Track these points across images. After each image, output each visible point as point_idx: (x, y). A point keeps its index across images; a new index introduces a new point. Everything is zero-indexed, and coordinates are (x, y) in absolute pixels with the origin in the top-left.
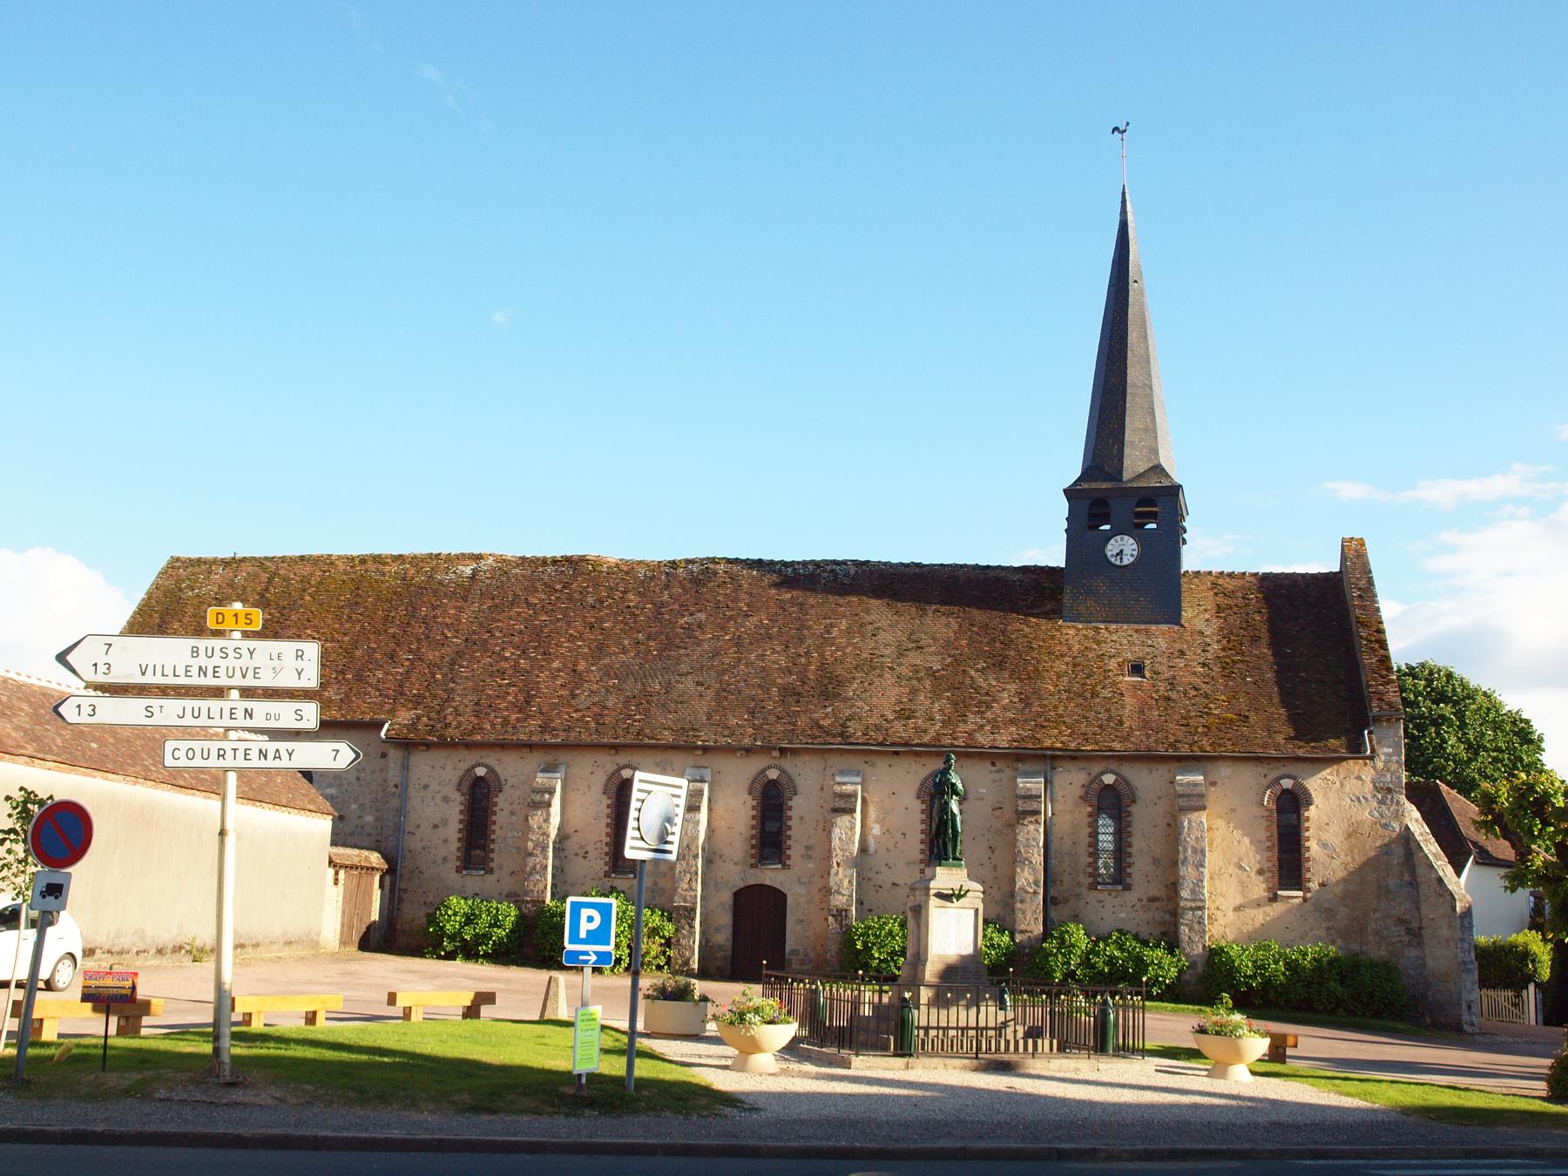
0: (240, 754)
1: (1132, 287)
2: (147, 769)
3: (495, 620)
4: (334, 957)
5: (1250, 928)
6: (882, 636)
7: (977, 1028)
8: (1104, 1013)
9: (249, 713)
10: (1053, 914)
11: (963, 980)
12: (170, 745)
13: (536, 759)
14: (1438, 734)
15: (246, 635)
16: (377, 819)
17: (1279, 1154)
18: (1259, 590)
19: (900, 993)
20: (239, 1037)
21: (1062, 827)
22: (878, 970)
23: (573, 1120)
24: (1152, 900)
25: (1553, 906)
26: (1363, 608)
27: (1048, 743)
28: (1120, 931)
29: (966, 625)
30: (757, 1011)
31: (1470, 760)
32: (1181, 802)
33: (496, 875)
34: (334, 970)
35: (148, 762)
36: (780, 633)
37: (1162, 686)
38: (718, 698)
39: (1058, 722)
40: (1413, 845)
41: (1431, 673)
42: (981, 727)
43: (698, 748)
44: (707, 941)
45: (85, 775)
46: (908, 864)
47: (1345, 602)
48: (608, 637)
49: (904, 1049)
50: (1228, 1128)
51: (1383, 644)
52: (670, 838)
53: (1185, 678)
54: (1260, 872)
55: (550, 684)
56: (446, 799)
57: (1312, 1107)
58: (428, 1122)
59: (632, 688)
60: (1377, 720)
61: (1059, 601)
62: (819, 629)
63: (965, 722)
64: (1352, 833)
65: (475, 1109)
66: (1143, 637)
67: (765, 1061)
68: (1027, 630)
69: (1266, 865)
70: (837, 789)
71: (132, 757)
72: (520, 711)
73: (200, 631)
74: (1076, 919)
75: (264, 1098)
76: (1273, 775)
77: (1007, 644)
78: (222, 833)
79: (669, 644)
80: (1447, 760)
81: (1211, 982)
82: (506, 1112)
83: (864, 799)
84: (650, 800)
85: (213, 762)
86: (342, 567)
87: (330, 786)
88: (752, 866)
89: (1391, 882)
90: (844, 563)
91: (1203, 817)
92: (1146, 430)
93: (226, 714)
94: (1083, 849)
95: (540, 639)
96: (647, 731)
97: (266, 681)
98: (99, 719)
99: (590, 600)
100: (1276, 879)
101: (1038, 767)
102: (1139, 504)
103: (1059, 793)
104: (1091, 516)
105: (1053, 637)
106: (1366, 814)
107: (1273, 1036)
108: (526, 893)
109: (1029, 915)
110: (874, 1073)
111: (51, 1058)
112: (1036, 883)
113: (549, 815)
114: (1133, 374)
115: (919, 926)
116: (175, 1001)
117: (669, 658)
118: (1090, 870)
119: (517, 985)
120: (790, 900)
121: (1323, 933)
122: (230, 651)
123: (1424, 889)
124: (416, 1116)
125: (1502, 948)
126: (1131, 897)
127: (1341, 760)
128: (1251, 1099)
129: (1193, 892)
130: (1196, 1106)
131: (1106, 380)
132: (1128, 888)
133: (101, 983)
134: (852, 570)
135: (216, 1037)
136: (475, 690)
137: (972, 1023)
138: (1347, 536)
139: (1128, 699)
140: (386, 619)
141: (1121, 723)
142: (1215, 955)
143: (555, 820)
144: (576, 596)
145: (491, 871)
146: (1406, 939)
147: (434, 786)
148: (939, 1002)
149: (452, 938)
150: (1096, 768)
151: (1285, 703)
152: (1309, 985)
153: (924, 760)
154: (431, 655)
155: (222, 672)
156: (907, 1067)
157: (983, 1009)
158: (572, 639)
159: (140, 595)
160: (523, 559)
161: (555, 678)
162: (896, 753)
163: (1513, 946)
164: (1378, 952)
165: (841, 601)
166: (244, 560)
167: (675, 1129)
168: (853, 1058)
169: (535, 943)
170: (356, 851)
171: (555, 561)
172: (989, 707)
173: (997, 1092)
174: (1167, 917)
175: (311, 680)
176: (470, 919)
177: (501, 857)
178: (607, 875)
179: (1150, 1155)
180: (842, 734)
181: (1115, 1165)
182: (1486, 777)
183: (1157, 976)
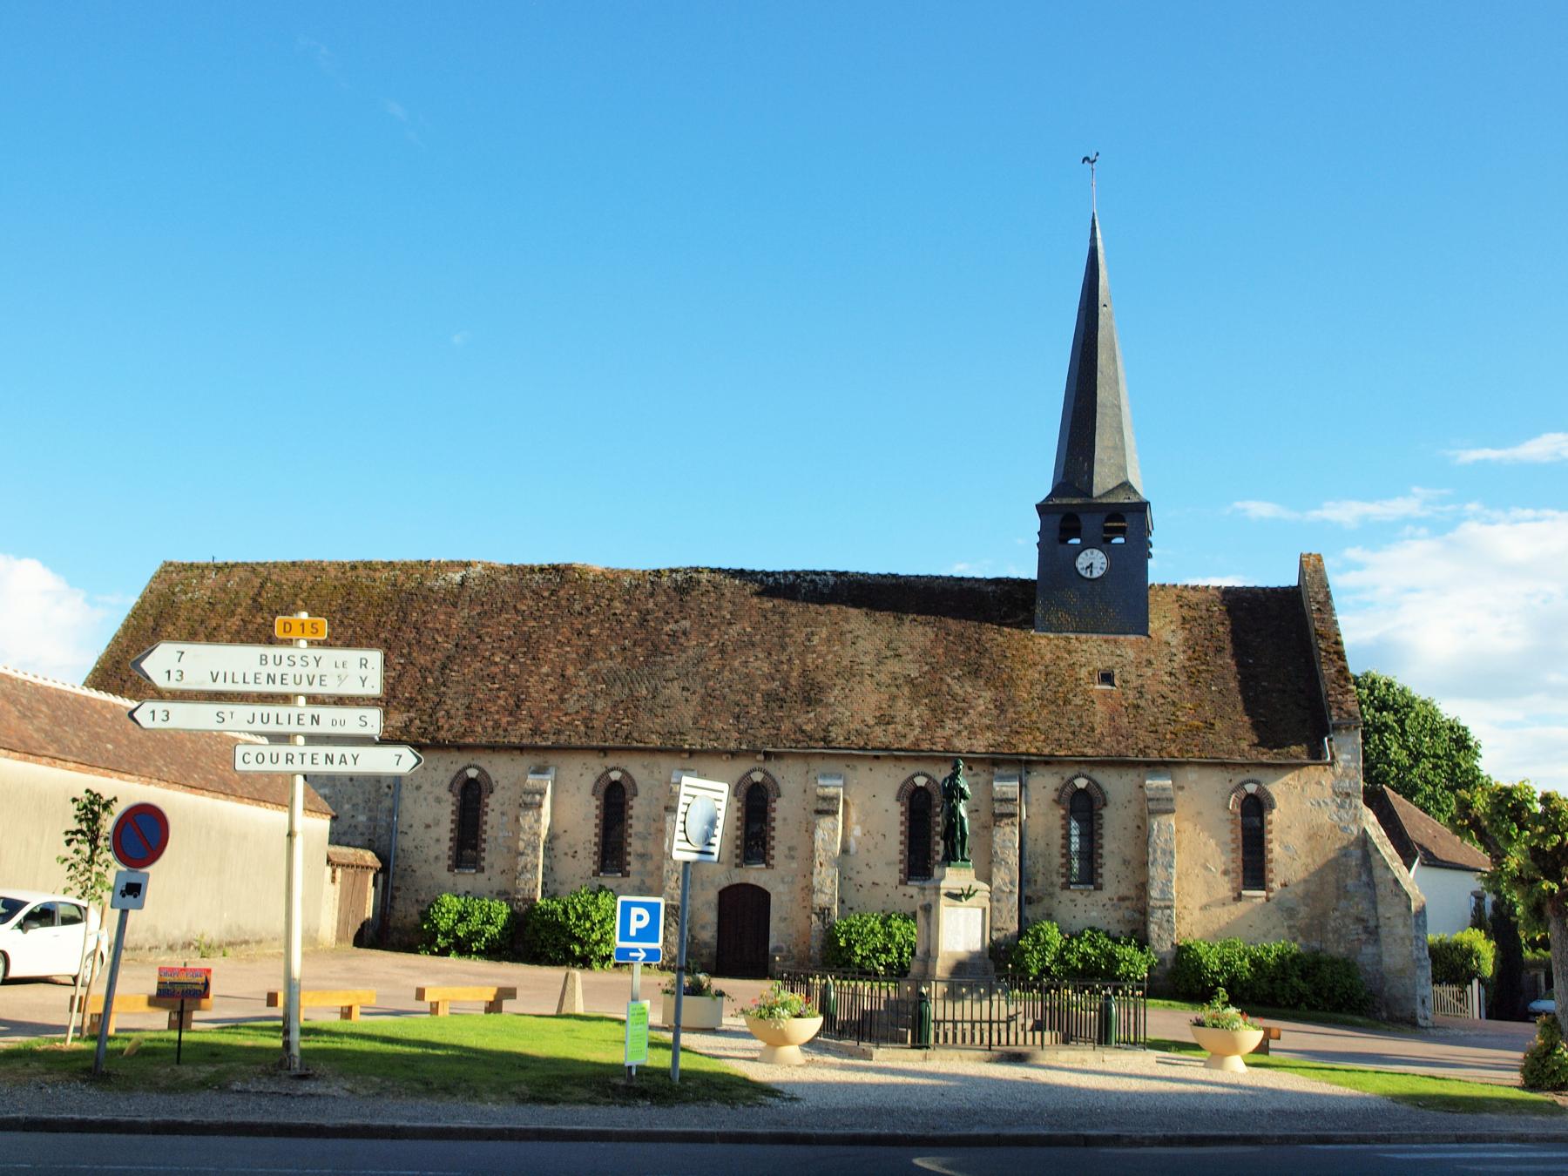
0: (308, 759)
2: (159, 770)
3: (483, 626)
4: (333, 953)
5: (1216, 927)
7: (954, 1022)
8: (1109, 1009)
9: (315, 720)
10: (1028, 913)
11: (973, 975)
12: (240, 750)
13: (527, 761)
14: (1381, 740)
15: (311, 643)
16: (370, 819)
17: (1285, 1140)
18: (1222, 602)
19: (918, 987)
21: (1036, 829)
22: (860, 966)
23: (628, 1110)
24: (1122, 899)
25: (1527, 907)
26: (1323, 621)
27: (1023, 748)
28: (1092, 929)
29: (942, 634)
30: (784, 1005)
31: (1412, 767)
32: (1151, 805)
33: (487, 873)
36: (763, 641)
37: (1131, 694)
38: (704, 704)
39: (1031, 729)
41: (1374, 682)
42: (959, 732)
44: (693, 938)
45: (103, 775)
46: (888, 864)
47: (1303, 615)
48: (595, 643)
49: (920, 1042)
50: (1235, 1116)
51: (1341, 655)
52: (713, 840)
53: (1153, 688)
54: (1225, 873)
55: (539, 688)
56: (438, 800)
57: (1309, 1095)
58: (495, 1112)
59: (618, 692)
60: (1336, 728)
61: (1032, 613)
62: (800, 638)
63: (942, 727)
64: (1313, 836)
65: (536, 1100)
66: (1112, 647)
67: (792, 1052)
68: (1000, 639)
69: (1231, 866)
70: (820, 791)
71: (145, 758)
72: (511, 714)
73: (271, 641)
74: (1049, 917)
75: (335, 1090)
78: (291, 835)
80: (1390, 765)
81: (1184, 980)
84: (696, 804)
85: (282, 766)
87: (324, 786)
88: (737, 866)
89: (1350, 882)
91: (1171, 820)
92: (1115, 448)
93: (294, 719)
94: (1056, 851)
95: (529, 645)
96: (635, 735)
97: (332, 688)
98: (173, 723)
99: (577, 607)
100: (1240, 879)
103: (1033, 799)
105: (1026, 647)
106: (1327, 816)
107: (1267, 1031)
108: (517, 892)
109: (1005, 913)
110: (892, 1066)
111: (121, 1051)
112: (1012, 883)
113: (540, 815)
114: (1102, 395)
115: (929, 924)
116: (235, 1000)
119: (535, 983)
120: (773, 899)
121: (1285, 931)
122: (297, 660)
124: (481, 1107)
125: (1448, 946)
129: (1162, 891)
130: (1202, 1095)
132: (1099, 888)
134: (832, 580)
136: (466, 694)
137: (986, 1017)
138: (1306, 552)
139: (1098, 707)
140: (378, 623)
141: (1093, 729)
144: (564, 603)
145: (482, 870)
146: (1364, 937)
147: (426, 787)
148: (953, 995)
149: (446, 935)
150: (1069, 773)
152: (1272, 980)
154: (423, 660)
155: (289, 680)
156: (925, 1058)
158: (560, 644)
159: (132, 600)
160: (511, 566)
162: (877, 757)
164: (1339, 950)
165: (821, 609)
166: (235, 565)
167: (724, 1118)
168: (875, 1050)
169: (538, 938)
170: (352, 850)
171: (542, 570)
172: (966, 713)
173: (1015, 1082)
174: (1136, 915)
175: (374, 687)
176: (462, 917)
177: (492, 856)
178: (595, 874)
179: (1168, 1141)
180: (824, 739)
181: (1134, 1151)
182: (1427, 782)
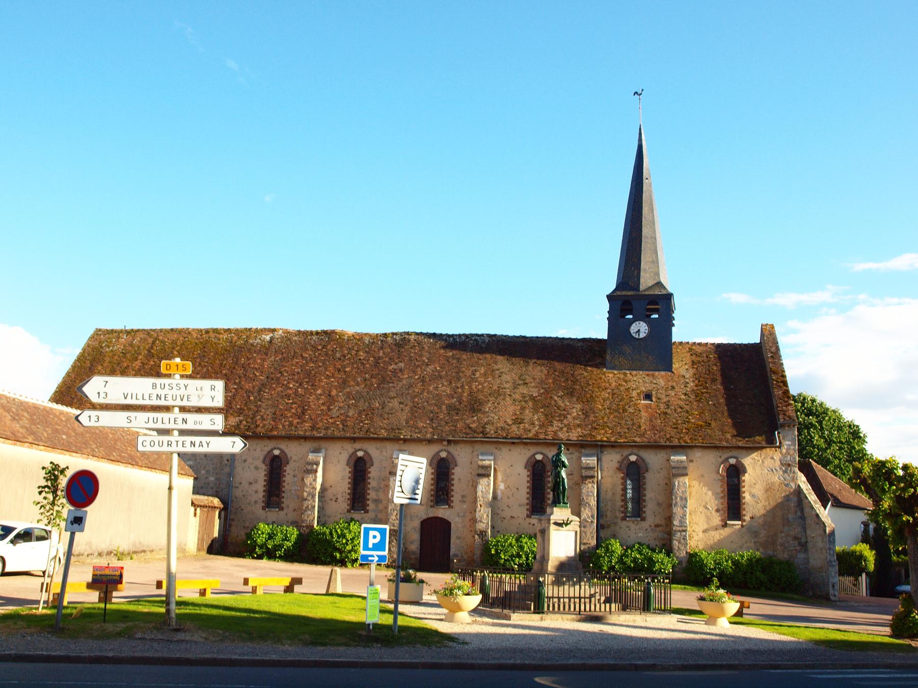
0: (180, 444)
1: (645, 182)
2: (93, 450)
3: (283, 366)
4: (195, 558)
5: (712, 542)
6: (504, 377)
9: (185, 421)
10: (602, 534)
11: (569, 571)
12: (141, 439)
13: (308, 445)
14: (809, 433)
15: (182, 376)
16: (216, 479)
18: (715, 353)
20: (180, 604)
21: (607, 484)
22: (504, 565)
23: (368, 649)
24: (657, 526)
26: (774, 363)
27: (599, 438)
29: (551, 371)
30: (459, 588)
31: (826, 449)
32: (674, 471)
33: (285, 511)
34: (198, 565)
35: (94, 446)
36: (447, 375)
37: (662, 406)
40: (802, 496)
41: (804, 399)
42: (562, 429)
43: (401, 439)
46: (520, 505)
47: (763, 360)
48: (348, 376)
49: (539, 610)
50: (723, 653)
51: (785, 383)
52: (417, 492)
53: (675, 402)
54: (717, 511)
55: (316, 402)
56: (257, 468)
57: (761, 640)
58: (290, 651)
59: (362, 405)
60: (783, 426)
61: (604, 359)
62: (469, 373)
63: (552, 426)
64: (768, 489)
65: (314, 643)
66: (651, 379)
67: (463, 616)
68: (586, 374)
69: (721, 507)
70: (480, 463)
71: (85, 444)
72: (299, 418)
73: (159, 375)
74: (614, 536)
75: (196, 638)
76: (724, 457)
77: (575, 382)
78: (170, 488)
79: (383, 380)
80: (814, 448)
81: (693, 573)
82: (331, 645)
83: (495, 469)
84: (407, 470)
85: (165, 448)
86: (195, 336)
87: (190, 460)
88: (432, 506)
89: (790, 516)
90: (482, 335)
91: (686, 480)
92: (653, 262)
93: (172, 421)
94: (618, 497)
95: (310, 377)
97: (194, 402)
98: (101, 423)
99: (338, 355)
101: (593, 451)
102: (649, 304)
104: (622, 310)
105: (600, 378)
106: (776, 478)
108: (303, 521)
110: (523, 623)
111: (71, 615)
112: (592, 516)
113: (316, 477)
114: (645, 231)
115: (544, 541)
116: (138, 582)
117: (383, 388)
118: (622, 509)
119: (314, 575)
120: (453, 526)
121: (752, 545)
122: (174, 386)
123: (808, 521)
124: (282, 648)
125: (848, 553)
126: (646, 525)
127: (762, 448)
128: (732, 636)
129: (680, 521)
130: (704, 640)
131: (631, 234)
132: (643, 519)
133: (103, 573)
135: (167, 603)
136: (273, 406)
137: (577, 595)
138: (764, 323)
139: (643, 414)
140: (221, 365)
141: (640, 427)
142: (692, 556)
143: (319, 480)
145: (282, 509)
146: (798, 548)
147: (250, 460)
148: (558, 582)
149: (261, 547)
150: (533, 450)
151: (731, 416)
152: (745, 573)
153: (529, 447)
154: (248, 386)
155: (169, 398)
156: (542, 619)
157: (583, 587)
158: (328, 377)
159: (77, 351)
160: (299, 331)
161: (318, 399)
162: (513, 443)
163: (854, 552)
164: (783, 556)
165: (481, 357)
166: (138, 331)
167: (424, 654)
170: (206, 498)
171: (317, 333)
174: (665, 536)
175: (219, 402)
176: (271, 536)
177: (288, 501)
178: (349, 511)
179: (684, 668)
180: (482, 432)
183: (661, 569)
